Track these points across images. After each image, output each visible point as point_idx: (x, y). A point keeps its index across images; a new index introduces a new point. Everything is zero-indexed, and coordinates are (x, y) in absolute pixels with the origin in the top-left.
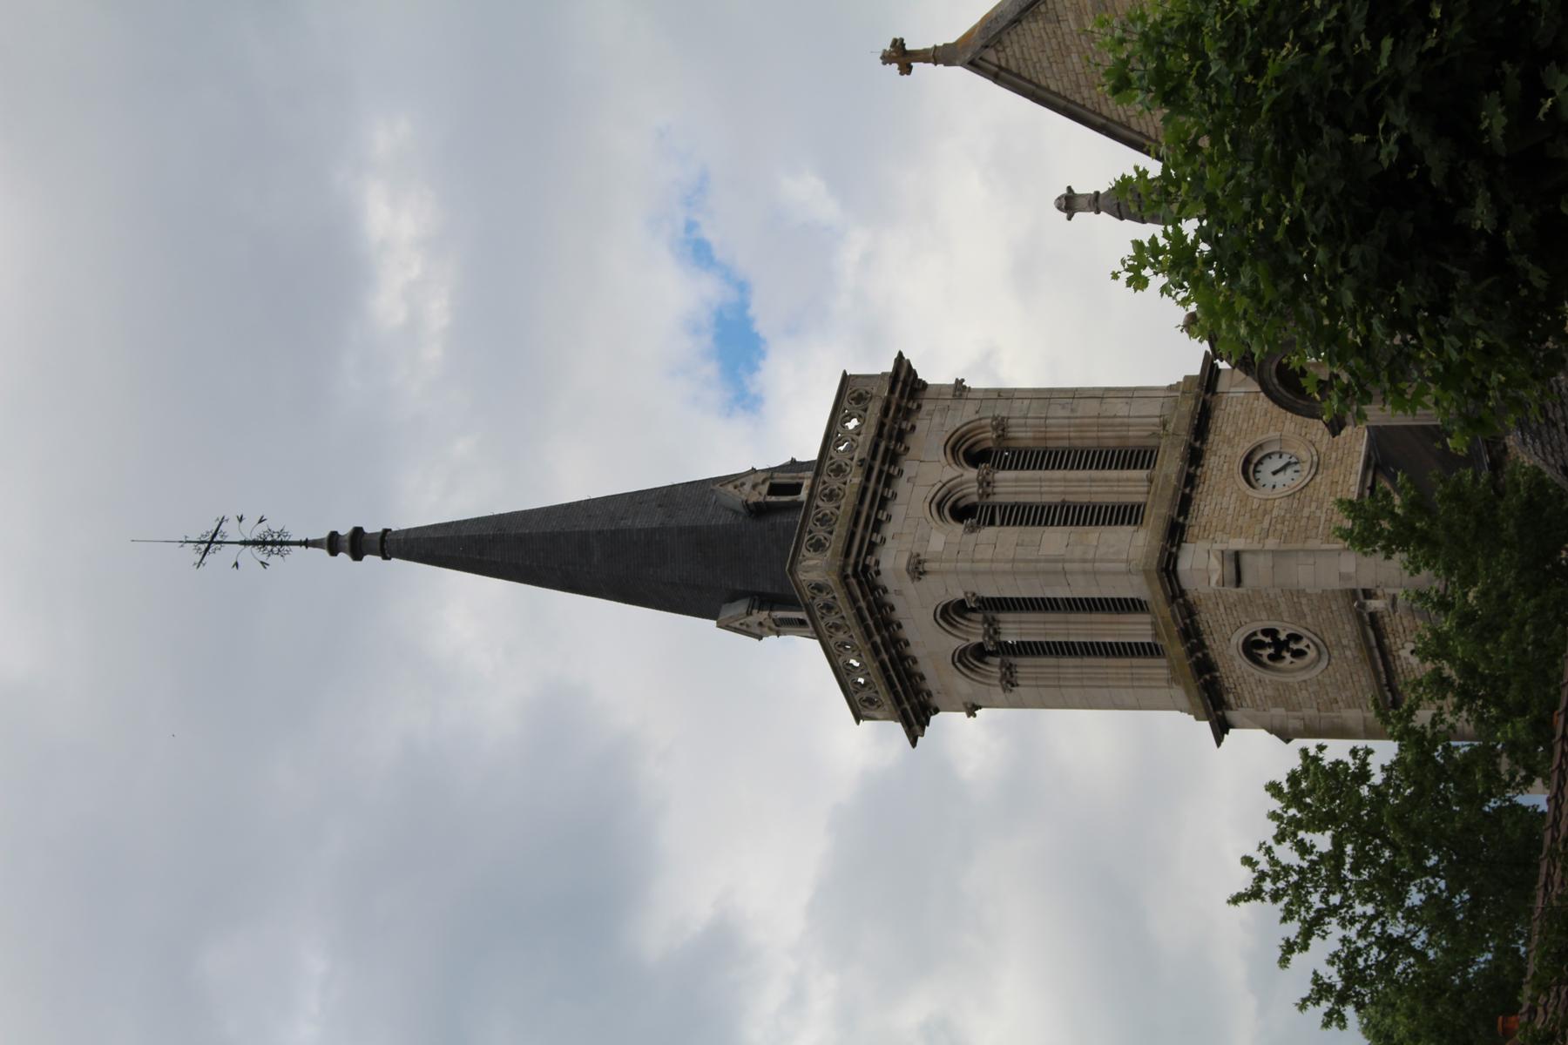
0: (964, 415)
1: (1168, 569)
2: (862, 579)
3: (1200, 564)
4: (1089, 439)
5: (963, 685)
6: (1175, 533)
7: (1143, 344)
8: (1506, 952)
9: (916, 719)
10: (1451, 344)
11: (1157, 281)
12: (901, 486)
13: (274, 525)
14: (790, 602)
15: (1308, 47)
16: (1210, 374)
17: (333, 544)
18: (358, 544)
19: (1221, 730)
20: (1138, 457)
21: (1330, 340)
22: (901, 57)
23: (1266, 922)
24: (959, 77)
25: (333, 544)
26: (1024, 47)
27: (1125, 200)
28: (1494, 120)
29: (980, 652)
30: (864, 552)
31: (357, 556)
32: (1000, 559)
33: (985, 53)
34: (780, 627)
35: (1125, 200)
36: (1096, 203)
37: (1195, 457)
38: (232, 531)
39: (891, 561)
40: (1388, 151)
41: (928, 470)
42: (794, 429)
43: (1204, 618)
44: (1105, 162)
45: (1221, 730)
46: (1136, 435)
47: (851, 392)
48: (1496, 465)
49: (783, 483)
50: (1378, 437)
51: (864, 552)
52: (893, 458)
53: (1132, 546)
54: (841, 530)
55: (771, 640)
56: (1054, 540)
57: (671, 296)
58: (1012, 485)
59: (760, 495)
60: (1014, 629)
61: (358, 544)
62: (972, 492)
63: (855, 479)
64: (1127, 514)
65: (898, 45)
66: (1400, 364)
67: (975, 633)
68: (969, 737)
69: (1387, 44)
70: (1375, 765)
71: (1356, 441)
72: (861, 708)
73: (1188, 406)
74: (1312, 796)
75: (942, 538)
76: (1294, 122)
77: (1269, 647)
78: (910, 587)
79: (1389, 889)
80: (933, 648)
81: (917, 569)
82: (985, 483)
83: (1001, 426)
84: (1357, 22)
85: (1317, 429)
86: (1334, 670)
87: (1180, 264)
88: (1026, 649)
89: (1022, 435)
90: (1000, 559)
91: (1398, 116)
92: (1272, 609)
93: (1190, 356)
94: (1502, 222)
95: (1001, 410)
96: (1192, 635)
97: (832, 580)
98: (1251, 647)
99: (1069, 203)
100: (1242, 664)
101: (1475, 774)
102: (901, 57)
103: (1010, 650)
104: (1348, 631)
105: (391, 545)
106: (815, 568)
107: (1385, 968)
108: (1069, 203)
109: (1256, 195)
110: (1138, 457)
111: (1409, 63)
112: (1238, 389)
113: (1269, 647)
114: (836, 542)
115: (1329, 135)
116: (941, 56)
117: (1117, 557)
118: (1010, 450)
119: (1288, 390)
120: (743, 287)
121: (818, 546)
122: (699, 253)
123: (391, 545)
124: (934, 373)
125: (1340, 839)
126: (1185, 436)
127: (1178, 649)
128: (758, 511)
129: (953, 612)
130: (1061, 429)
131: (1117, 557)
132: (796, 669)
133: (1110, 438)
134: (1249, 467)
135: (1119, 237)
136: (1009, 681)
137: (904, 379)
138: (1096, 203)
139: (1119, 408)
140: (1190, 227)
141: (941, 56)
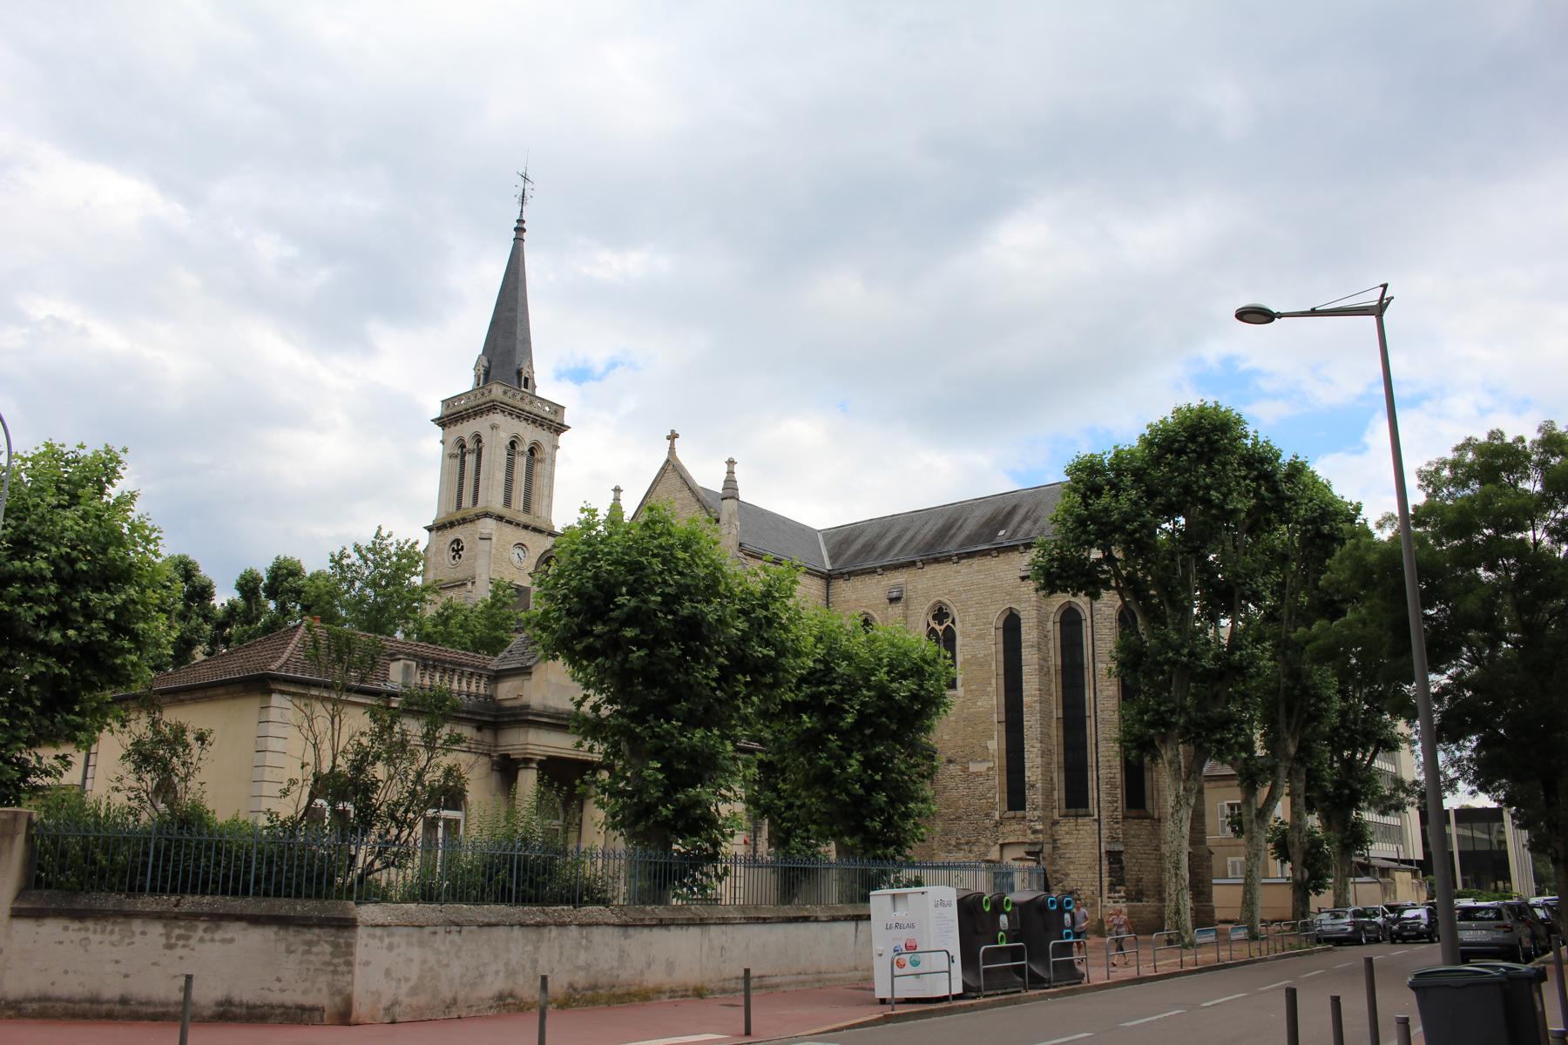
0: (547, 447)
1: (487, 515)
2: (492, 407)
3: (488, 526)
4: (535, 490)
5: (452, 439)
6: (500, 518)
7: (564, 514)
8: (345, 621)
9: (442, 422)
10: (556, 614)
11: (582, 516)
12: (524, 424)
13: (529, 201)
14: (486, 380)
15: (661, 573)
16: (552, 534)
17: (521, 221)
18: (520, 230)
19: (430, 529)
20: (527, 508)
21: (560, 575)
22: (673, 437)
23: (366, 540)
24: (665, 456)
25: (521, 221)
26: (672, 480)
27: (616, 508)
28: (629, 633)
29: (463, 446)
30: (501, 403)
31: (516, 229)
32: (495, 456)
33: (671, 467)
34: (478, 377)
35: (616, 508)
36: (617, 499)
37: (526, 527)
38: (528, 186)
39: (497, 418)
40: (620, 600)
41: (529, 433)
42: (547, 386)
43: (469, 526)
44: (629, 507)
45: (430, 529)
46: (535, 507)
47: (558, 409)
48: (517, 630)
49: (526, 382)
50: (527, 590)
51: (501, 403)
52: (534, 422)
53: (497, 505)
54: (510, 401)
55: (473, 373)
56: (501, 476)
57: (597, 354)
58: (521, 463)
59: (525, 374)
60: (470, 459)
61: (520, 230)
62: (519, 448)
63: (527, 408)
64: (508, 502)
65: (677, 436)
66: (551, 598)
67: (470, 445)
68: (433, 444)
69: (659, 599)
70: (414, 579)
71: (526, 582)
72: (446, 403)
73: (544, 526)
74: (409, 557)
75: (504, 437)
76: (635, 568)
77: (457, 548)
78: (488, 424)
79: (374, 584)
80: (466, 430)
81: (494, 427)
82: (523, 453)
83: (542, 461)
84: (668, 590)
85: (531, 569)
86: (444, 568)
87: (589, 525)
88: (463, 463)
89: (538, 468)
90: (495, 456)
91: (633, 603)
92: (470, 550)
93: (558, 529)
94: (598, 637)
95: (548, 461)
96: (464, 521)
97: (493, 396)
98: (458, 541)
99: (617, 490)
100: (452, 538)
101: (407, 613)
102: (673, 437)
103: (464, 455)
104: (461, 576)
105: (519, 241)
106: (497, 391)
107: (344, 579)
108: (617, 490)
109: (610, 553)
110: (527, 508)
111: (652, 606)
112: (548, 543)
113: (457, 548)
114: (506, 399)
115: (631, 578)
116: (672, 449)
117: (492, 498)
118: (532, 461)
119: (546, 559)
120: (599, 379)
121: (505, 393)
122: (612, 365)
123: (519, 241)
124: (563, 438)
125: (391, 570)
126: (533, 524)
127: (459, 516)
128: (519, 373)
129: (478, 439)
130: (538, 482)
131: (492, 498)
132: (463, 381)
133: (534, 498)
134: (521, 545)
135: (603, 513)
136: (452, 456)
137: (560, 428)
138: (617, 499)
139: (545, 503)
140: (600, 528)
141: (672, 449)
